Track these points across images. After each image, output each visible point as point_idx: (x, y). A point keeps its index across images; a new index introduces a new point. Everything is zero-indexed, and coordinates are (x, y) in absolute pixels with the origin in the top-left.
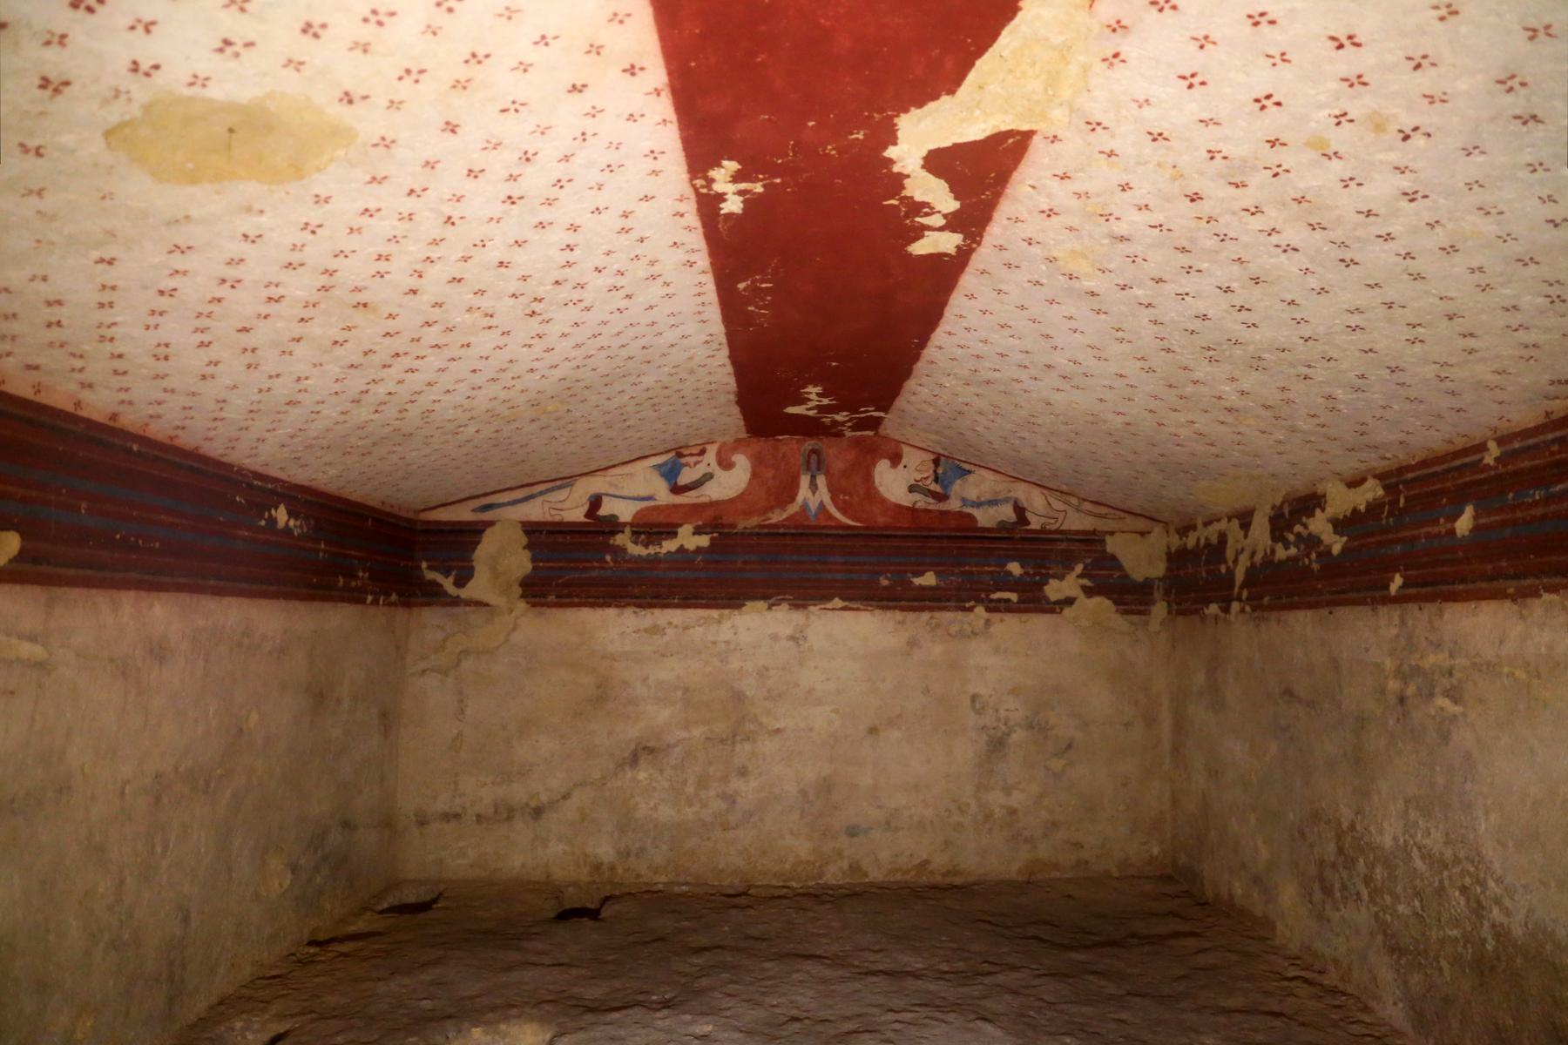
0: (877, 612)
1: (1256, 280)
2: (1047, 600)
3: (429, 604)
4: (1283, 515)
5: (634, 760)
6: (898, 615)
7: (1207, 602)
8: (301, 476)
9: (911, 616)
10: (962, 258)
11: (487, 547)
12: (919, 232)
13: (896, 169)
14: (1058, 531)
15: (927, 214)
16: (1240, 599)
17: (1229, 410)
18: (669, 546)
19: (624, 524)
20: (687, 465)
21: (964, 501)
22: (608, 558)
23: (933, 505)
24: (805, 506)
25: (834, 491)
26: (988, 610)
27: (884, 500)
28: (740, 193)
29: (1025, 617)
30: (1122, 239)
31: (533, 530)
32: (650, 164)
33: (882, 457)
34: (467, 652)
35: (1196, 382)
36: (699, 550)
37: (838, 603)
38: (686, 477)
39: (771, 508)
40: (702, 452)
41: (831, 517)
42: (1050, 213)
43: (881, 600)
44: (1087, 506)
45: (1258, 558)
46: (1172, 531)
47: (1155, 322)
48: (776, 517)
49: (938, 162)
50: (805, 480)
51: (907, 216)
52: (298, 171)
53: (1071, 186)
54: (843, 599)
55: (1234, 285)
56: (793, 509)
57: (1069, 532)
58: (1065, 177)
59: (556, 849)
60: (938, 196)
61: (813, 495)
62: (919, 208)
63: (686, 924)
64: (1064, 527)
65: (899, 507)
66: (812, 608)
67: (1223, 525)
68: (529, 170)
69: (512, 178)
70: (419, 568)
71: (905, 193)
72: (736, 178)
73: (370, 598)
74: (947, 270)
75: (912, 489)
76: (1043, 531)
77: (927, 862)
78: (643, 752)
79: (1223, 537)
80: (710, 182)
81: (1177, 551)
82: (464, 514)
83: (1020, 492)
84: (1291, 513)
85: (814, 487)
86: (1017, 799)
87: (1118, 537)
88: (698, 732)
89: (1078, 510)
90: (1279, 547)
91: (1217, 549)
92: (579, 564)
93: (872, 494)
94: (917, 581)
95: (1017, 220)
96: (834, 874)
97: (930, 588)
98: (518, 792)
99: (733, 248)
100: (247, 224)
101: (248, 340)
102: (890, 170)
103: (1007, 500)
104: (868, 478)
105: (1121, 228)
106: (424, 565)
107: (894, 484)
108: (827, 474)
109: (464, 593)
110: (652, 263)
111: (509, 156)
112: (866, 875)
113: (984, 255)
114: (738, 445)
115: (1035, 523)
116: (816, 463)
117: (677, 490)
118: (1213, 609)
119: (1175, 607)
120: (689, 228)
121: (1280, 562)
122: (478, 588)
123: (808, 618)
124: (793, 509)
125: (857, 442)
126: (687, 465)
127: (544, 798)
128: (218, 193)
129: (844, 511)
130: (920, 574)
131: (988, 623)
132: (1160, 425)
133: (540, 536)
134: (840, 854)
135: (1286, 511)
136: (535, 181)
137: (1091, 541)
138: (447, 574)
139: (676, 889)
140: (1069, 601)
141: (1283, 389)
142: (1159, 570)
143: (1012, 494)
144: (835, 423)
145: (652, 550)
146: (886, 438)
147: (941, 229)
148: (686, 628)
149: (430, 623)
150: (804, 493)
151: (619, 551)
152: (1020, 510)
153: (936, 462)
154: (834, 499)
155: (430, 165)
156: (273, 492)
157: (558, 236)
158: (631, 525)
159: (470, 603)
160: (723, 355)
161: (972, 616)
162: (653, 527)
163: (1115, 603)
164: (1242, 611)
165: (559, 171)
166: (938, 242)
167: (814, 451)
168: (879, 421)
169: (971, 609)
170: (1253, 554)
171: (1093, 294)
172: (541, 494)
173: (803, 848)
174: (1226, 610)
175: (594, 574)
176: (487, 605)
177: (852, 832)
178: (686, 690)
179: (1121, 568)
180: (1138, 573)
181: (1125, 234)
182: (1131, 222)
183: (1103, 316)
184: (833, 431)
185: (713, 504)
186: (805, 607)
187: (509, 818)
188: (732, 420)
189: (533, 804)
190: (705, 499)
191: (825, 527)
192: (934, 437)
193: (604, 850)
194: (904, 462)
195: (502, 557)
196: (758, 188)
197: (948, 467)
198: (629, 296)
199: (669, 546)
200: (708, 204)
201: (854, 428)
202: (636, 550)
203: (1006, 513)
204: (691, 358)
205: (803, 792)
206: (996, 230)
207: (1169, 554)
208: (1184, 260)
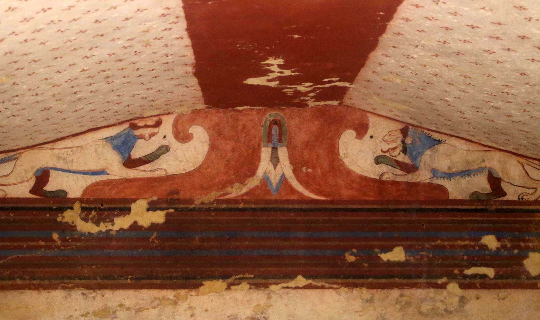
0: (343, 290)
2: (529, 276)
6: (366, 293)
9: (379, 294)
18: (122, 223)
19: (74, 200)
20: (142, 137)
21: (435, 172)
22: (55, 236)
24: (265, 181)
25: (293, 161)
26: (463, 286)
27: (349, 172)
29: (503, 293)
33: (346, 127)
36: (154, 227)
37: (301, 281)
39: (230, 183)
40: (158, 124)
41: (293, 191)
48: (236, 191)
50: (265, 153)
54: (307, 277)
56: (253, 183)
61: (274, 169)
66: (273, 287)
75: (378, 160)
76: (521, 201)
85: (275, 160)
93: (336, 166)
94: (385, 257)
103: (480, 170)
114: (195, 116)
116: (278, 134)
117: (130, 163)
123: (269, 298)
124: (253, 183)
125: (321, 112)
126: (142, 137)
129: (306, 184)
143: (487, 164)
144: (297, 94)
145: (103, 227)
146: (352, 109)
148: (139, 310)
150: (264, 166)
151: (72, 228)
152: (495, 181)
153: (404, 132)
154: (295, 171)
160: (181, 28)
162: (104, 203)
167: (275, 122)
169: (443, 286)
175: (40, 253)
184: (296, 102)
185: (170, 178)
188: (191, 91)
190: (160, 174)
194: (370, 132)
197: (417, 137)
199: (122, 223)
201: (317, 98)
203: (481, 183)
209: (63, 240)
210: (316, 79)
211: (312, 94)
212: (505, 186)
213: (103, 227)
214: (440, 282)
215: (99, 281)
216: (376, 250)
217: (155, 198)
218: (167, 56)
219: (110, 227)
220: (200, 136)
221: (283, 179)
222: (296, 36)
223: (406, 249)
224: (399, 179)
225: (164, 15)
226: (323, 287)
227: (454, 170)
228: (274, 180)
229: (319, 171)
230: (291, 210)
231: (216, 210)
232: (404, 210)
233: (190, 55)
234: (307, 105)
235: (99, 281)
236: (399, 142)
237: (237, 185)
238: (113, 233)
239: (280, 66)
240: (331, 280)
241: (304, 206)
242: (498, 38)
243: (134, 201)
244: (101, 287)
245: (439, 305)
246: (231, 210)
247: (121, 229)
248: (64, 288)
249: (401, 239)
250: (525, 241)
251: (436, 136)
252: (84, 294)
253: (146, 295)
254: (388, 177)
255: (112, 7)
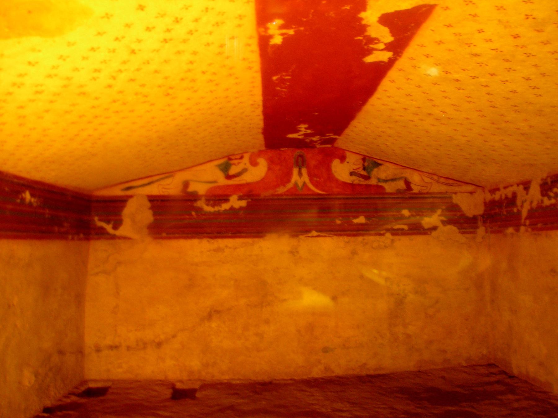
0: (335, 237)
1: (543, 75)
2: (424, 229)
3: (99, 239)
4: (547, 183)
5: (210, 317)
6: (346, 239)
7: (507, 226)
8: (37, 176)
9: (352, 239)
10: (391, 63)
11: (128, 211)
12: (370, 52)
13: (364, 22)
14: (427, 193)
15: (376, 43)
16: (525, 225)
17: (523, 134)
18: (225, 206)
19: (202, 196)
20: (234, 164)
21: (379, 180)
22: (193, 213)
23: (363, 182)
24: (296, 185)
25: (311, 176)
26: (393, 234)
27: (337, 180)
28: (282, 34)
29: (412, 237)
30: (476, 55)
31: (152, 199)
32: (238, 22)
33: (335, 158)
34: (119, 263)
35: (506, 122)
36: (241, 208)
37: (314, 233)
38: (233, 170)
39: (277, 186)
40: (242, 158)
41: (309, 189)
42: (440, 43)
43: (338, 231)
44: (442, 180)
45: (534, 205)
46: (487, 191)
47: (489, 94)
48: (281, 190)
49: (387, 20)
50: (295, 171)
51: (366, 44)
52: (60, 31)
53: (452, 30)
54: (317, 231)
55: (532, 77)
56: (290, 186)
57: (434, 193)
58: (449, 26)
59: (169, 363)
60: (385, 35)
61: (300, 179)
62: (371, 40)
63: (242, 401)
64: (431, 191)
65: (345, 184)
66: (301, 237)
67: (515, 188)
68: (178, 26)
69: (168, 30)
70: (93, 220)
71: (367, 34)
72: (281, 27)
73: (70, 237)
74: (381, 70)
75: (352, 174)
76: (420, 193)
77: (365, 364)
78: (213, 313)
79: (514, 195)
80: (267, 29)
81: (490, 201)
82: (117, 192)
83: (407, 174)
84: (552, 182)
85: (300, 174)
86: (411, 330)
87: (459, 195)
88: (243, 302)
89: (438, 182)
90: (546, 200)
91: (512, 200)
92: (177, 217)
93: (331, 177)
94: (356, 221)
95: (422, 46)
96: (317, 372)
97: (362, 224)
98: (148, 335)
99: (273, 61)
100: (32, 57)
101: (22, 112)
102: (360, 23)
103: (401, 178)
104: (329, 169)
105: (475, 50)
106: (96, 219)
107: (342, 171)
108: (308, 168)
109: (118, 233)
110: (231, 68)
111: (168, 20)
112: (333, 372)
113: (403, 62)
114: (260, 153)
115: (416, 189)
116: (301, 162)
117: (229, 177)
118: (510, 230)
119: (489, 229)
120: (252, 52)
121: (547, 206)
122: (122, 231)
123: (299, 242)
124: (290, 186)
125: (322, 151)
126: (234, 164)
127: (162, 337)
128: (19, 43)
129: (316, 185)
130: (357, 217)
131: (393, 241)
132: (485, 141)
133: (158, 203)
134: (319, 362)
135: (549, 181)
136: (180, 31)
137: (444, 198)
138: (108, 222)
139: (234, 382)
140: (435, 228)
141: (552, 125)
142: (480, 211)
143: (404, 175)
144: (312, 141)
145: (216, 209)
146: (338, 149)
147: (382, 50)
148: (236, 248)
149: (98, 249)
150: (295, 177)
151: (200, 209)
152: (408, 183)
153: (364, 160)
154: (311, 180)
155: (128, 26)
156: (23, 185)
157: (187, 57)
158: (206, 196)
159: (120, 238)
160: (259, 111)
161: (382, 238)
162: (218, 197)
163: (458, 229)
164: (527, 231)
165: (192, 26)
166: (380, 56)
167: (300, 156)
168: (334, 140)
169: (383, 235)
170: (531, 202)
171: (457, 80)
172: (157, 181)
173: (300, 360)
174: (517, 230)
175: (186, 222)
176: (130, 239)
177: (326, 350)
178: (236, 280)
179: (460, 210)
180: (470, 213)
181: (478, 52)
182: (482, 47)
183: (461, 91)
184: (310, 146)
185: (248, 184)
186: (297, 236)
187: (145, 348)
188: (259, 140)
189: (157, 340)
190: (243, 182)
191: (305, 195)
192: (362, 147)
193: (195, 363)
194: (347, 160)
195: (137, 214)
196: (291, 32)
197: (370, 163)
198: (217, 85)
199: (225, 206)
200: (264, 41)
201: (321, 144)
202: (208, 209)
203: (401, 185)
204: (243, 113)
205: (299, 331)
206: (411, 51)
207: (485, 203)
208: (507, 65)
209: (197, 215)
210: (322, 134)
211: (319, 142)
212: (413, 186)
213: (216, 209)
214: (382, 232)
215: (215, 235)
216: (351, 218)
217: (241, 194)
218: (250, 124)
219: (220, 209)
220: (263, 163)
221: (305, 184)
222: (316, 114)
223: (366, 217)
224: (362, 183)
225: (252, 105)
226: (325, 236)
227: (388, 178)
228: (300, 184)
229: (322, 179)
230: (309, 199)
231: (272, 199)
232: (364, 198)
233: (261, 124)
234: (316, 147)
235: (215, 235)
236: (361, 165)
237: (282, 187)
238: (221, 212)
239: (306, 128)
240: (329, 233)
241: (315, 197)
242: (417, 114)
243: (230, 195)
244: (216, 237)
245: (381, 243)
246: (279, 199)
247: (226, 210)
248: (199, 238)
249: (364, 212)
250: (422, 212)
251: (379, 162)
252: (208, 241)
253: (238, 241)
254: (356, 182)
255: (33, 65)
